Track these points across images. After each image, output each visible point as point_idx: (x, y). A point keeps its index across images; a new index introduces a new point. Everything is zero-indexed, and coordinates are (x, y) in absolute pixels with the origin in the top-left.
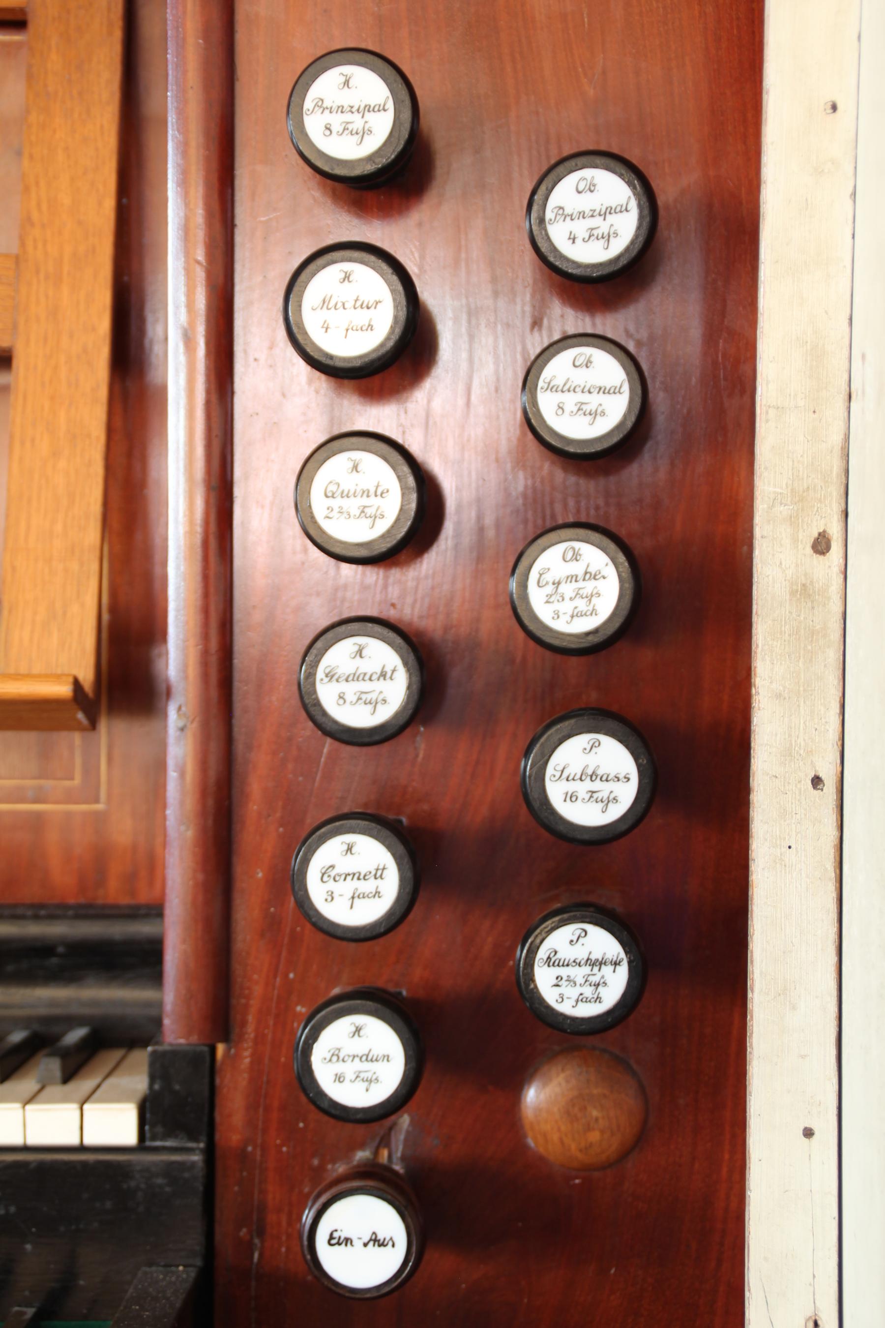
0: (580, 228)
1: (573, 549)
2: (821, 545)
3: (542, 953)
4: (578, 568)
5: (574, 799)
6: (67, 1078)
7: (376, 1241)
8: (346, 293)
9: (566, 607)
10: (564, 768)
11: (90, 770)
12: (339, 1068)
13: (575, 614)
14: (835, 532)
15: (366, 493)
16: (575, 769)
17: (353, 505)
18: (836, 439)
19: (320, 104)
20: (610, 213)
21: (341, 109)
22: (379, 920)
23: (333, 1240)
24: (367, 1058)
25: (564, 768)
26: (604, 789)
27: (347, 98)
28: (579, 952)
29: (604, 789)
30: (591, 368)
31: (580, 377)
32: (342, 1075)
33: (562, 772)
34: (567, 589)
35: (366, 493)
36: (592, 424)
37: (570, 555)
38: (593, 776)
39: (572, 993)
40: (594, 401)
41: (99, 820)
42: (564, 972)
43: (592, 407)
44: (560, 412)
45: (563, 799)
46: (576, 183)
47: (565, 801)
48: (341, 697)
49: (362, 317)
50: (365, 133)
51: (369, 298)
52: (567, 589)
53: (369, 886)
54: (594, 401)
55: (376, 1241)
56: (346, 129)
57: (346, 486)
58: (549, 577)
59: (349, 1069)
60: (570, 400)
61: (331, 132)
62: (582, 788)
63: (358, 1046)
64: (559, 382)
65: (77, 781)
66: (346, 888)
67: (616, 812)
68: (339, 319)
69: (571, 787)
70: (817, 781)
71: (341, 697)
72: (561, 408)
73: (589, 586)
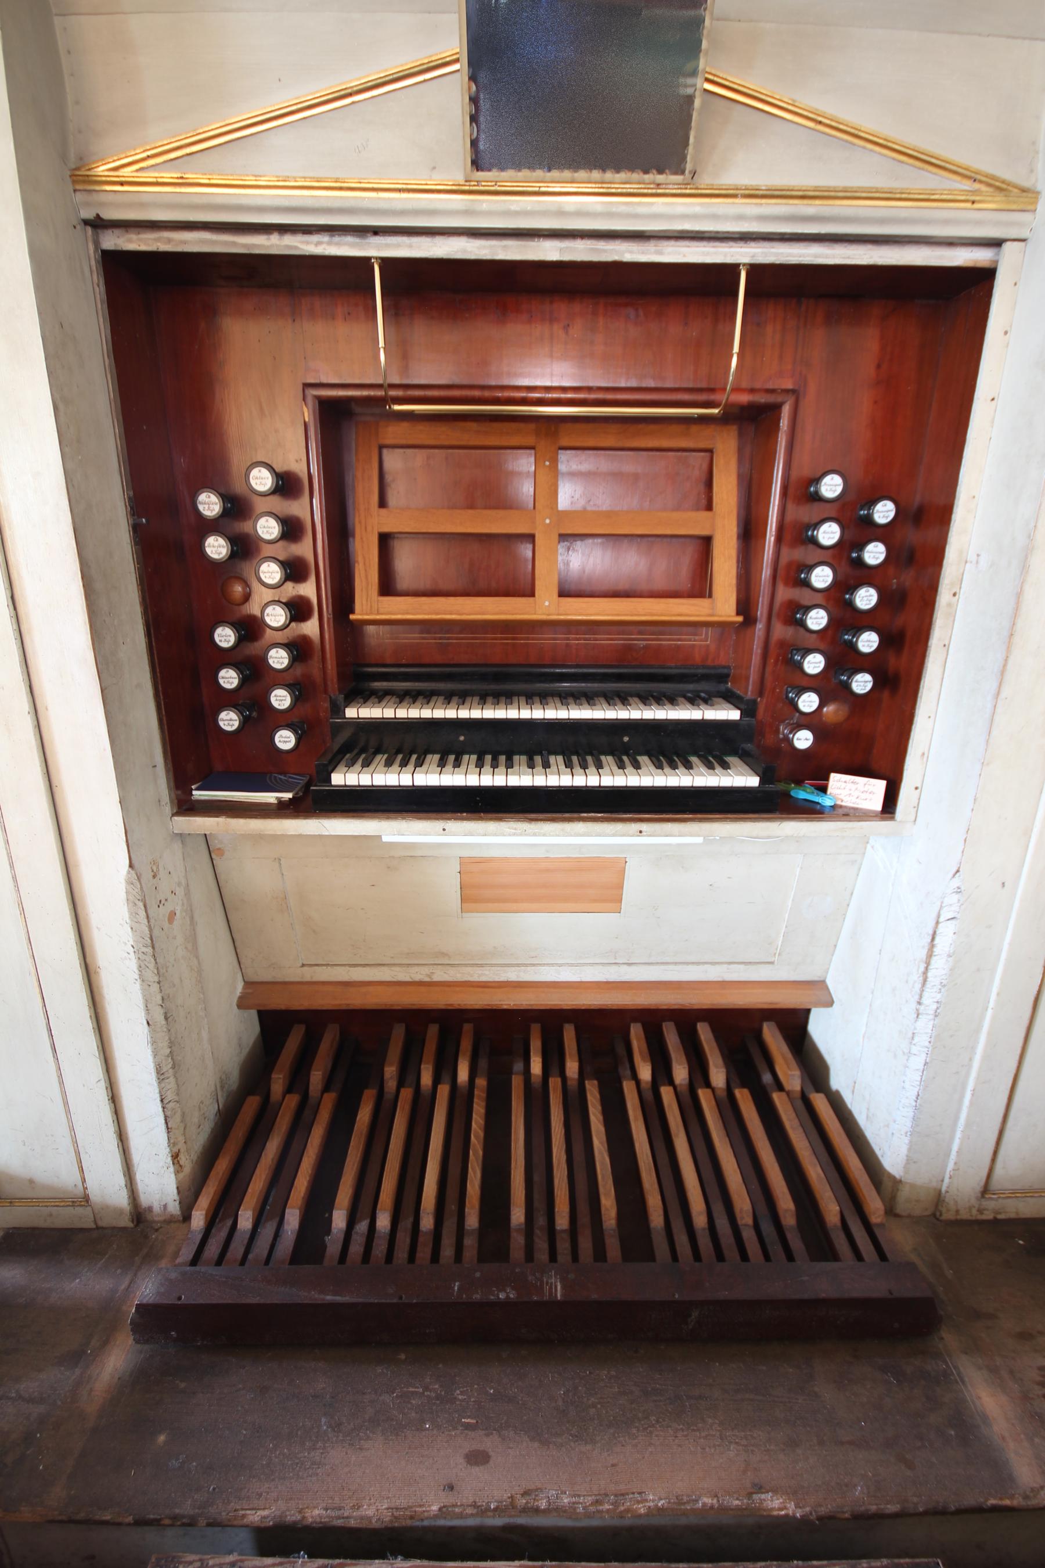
0: (882, 515)
2: (954, 595)
3: (855, 680)
4: (868, 594)
6: (379, 702)
7: (807, 739)
8: (830, 530)
9: (864, 603)
11: (707, 634)
12: (804, 704)
14: (958, 592)
15: (825, 576)
16: (865, 640)
17: (821, 579)
18: (962, 571)
19: (825, 484)
21: (831, 485)
23: (798, 739)
24: (811, 702)
26: (871, 644)
27: (832, 482)
28: (863, 679)
29: (871, 644)
31: (875, 550)
34: (865, 599)
35: (825, 576)
38: (869, 641)
39: (860, 688)
40: (877, 555)
41: (708, 646)
42: (859, 683)
49: (832, 536)
50: (835, 491)
51: (834, 531)
52: (865, 599)
53: (818, 665)
54: (877, 555)
55: (807, 739)
56: (831, 490)
57: (820, 575)
58: (862, 596)
59: (807, 704)
60: (872, 555)
62: (866, 644)
63: (809, 699)
64: (870, 550)
65: (704, 636)
66: (812, 665)
67: (873, 649)
68: (827, 536)
69: (864, 643)
70: (945, 646)
73: (871, 598)
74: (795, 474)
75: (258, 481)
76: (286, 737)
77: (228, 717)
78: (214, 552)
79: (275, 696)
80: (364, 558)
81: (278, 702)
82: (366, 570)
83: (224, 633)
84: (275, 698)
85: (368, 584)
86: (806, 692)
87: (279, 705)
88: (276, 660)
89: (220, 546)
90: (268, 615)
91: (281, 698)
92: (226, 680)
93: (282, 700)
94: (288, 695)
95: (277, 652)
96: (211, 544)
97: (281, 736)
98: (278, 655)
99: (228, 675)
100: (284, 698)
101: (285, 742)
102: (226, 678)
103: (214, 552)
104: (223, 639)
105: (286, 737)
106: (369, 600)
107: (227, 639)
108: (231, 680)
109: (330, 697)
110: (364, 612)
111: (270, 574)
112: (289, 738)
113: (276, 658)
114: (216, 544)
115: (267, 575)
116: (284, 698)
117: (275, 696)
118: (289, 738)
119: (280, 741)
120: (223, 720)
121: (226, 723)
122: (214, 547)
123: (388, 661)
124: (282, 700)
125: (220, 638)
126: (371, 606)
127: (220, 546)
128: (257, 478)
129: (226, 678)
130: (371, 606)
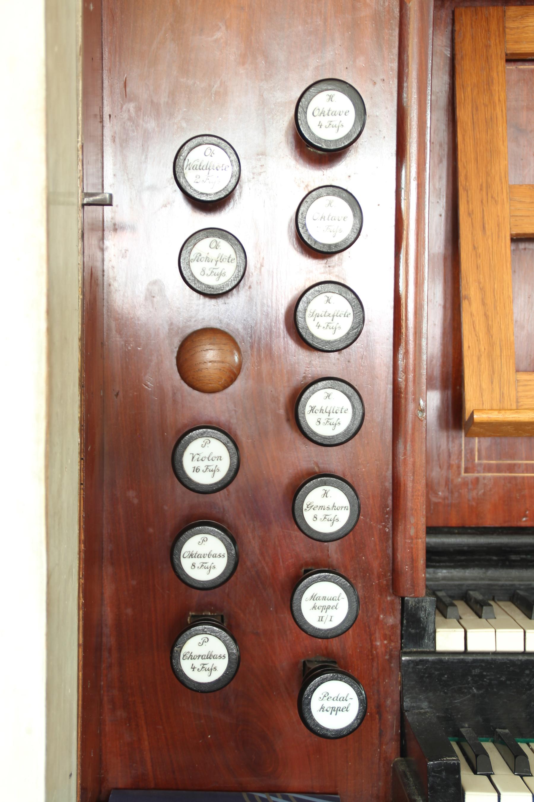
1: (216, 242)
5: (198, 471)
10: (314, 312)
13: (335, 314)
20: (339, 711)
22: (188, 677)
25: (314, 312)
30: (219, 249)
32: (198, 468)
33: (313, 313)
36: (210, 675)
37: (214, 245)
40: (332, 513)
43: (332, 517)
44: (193, 567)
45: (193, 471)
46: (209, 244)
47: (194, 472)
48: (193, 565)
61: (195, 567)
71: (193, 565)
72: (193, 565)
74: (431, 252)
75: (325, 120)
76: (337, 699)
77: (204, 650)
78: (208, 272)
79: (313, 598)
80: (482, 289)
81: (318, 613)
82: (486, 316)
83: (205, 452)
84: (312, 603)
85: (491, 345)
86: (225, 673)
87: (321, 619)
88: (320, 514)
89: (221, 259)
90: (312, 410)
91: (326, 603)
92: (198, 561)
93: (327, 608)
94: (344, 595)
95: (326, 494)
96: (204, 255)
97: (326, 696)
98: (327, 502)
99: (203, 549)
100: (332, 603)
101: (335, 710)
102: (199, 556)
103: (208, 272)
104: (202, 465)
105: (337, 699)
106: (496, 381)
107: (213, 464)
108: (210, 561)
109: (403, 602)
110: (487, 406)
111: (329, 319)
112: (345, 699)
113: (322, 508)
114: (214, 254)
115: (323, 321)
116: (332, 603)
117: (313, 598)
118: (345, 699)
119: (322, 708)
120: (191, 657)
121: (198, 663)
122: (208, 260)
123: (489, 522)
124: (327, 608)
125: (196, 464)
126: (502, 395)
127: (221, 259)
128: (323, 114)
129: (199, 556)
130: (502, 395)
